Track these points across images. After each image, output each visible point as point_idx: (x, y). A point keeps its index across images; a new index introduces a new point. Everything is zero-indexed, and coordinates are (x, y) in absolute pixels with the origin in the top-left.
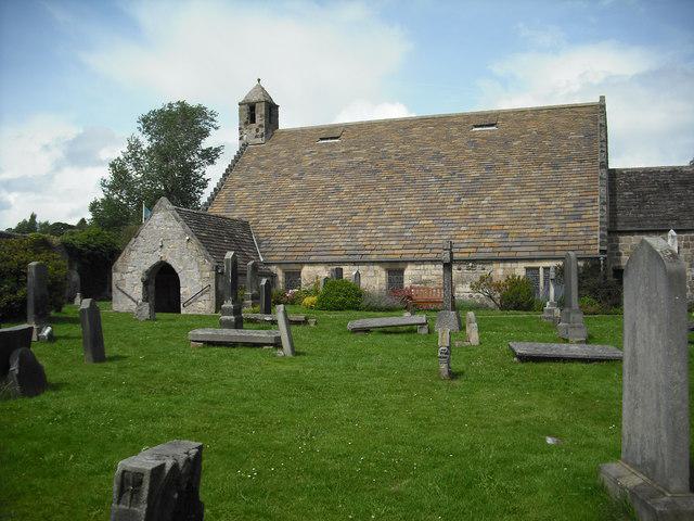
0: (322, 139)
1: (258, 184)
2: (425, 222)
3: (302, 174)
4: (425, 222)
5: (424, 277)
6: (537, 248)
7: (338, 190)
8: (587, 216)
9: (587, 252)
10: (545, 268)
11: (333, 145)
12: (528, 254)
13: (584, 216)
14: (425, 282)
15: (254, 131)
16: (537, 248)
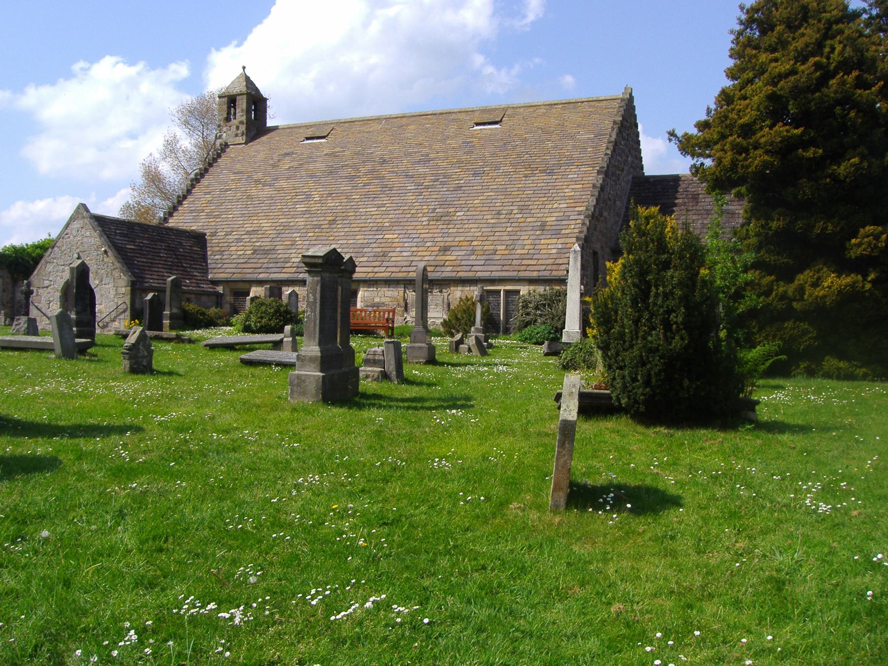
0: (308, 139)
1: (227, 190)
2: (391, 236)
3: (276, 179)
4: (391, 236)
5: (377, 300)
6: (499, 268)
7: (309, 197)
8: (568, 231)
9: (554, 273)
10: (507, 292)
11: (317, 147)
12: (515, 274)
13: (563, 232)
14: (378, 305)
15: (234, 128)
16: (499, 268)
